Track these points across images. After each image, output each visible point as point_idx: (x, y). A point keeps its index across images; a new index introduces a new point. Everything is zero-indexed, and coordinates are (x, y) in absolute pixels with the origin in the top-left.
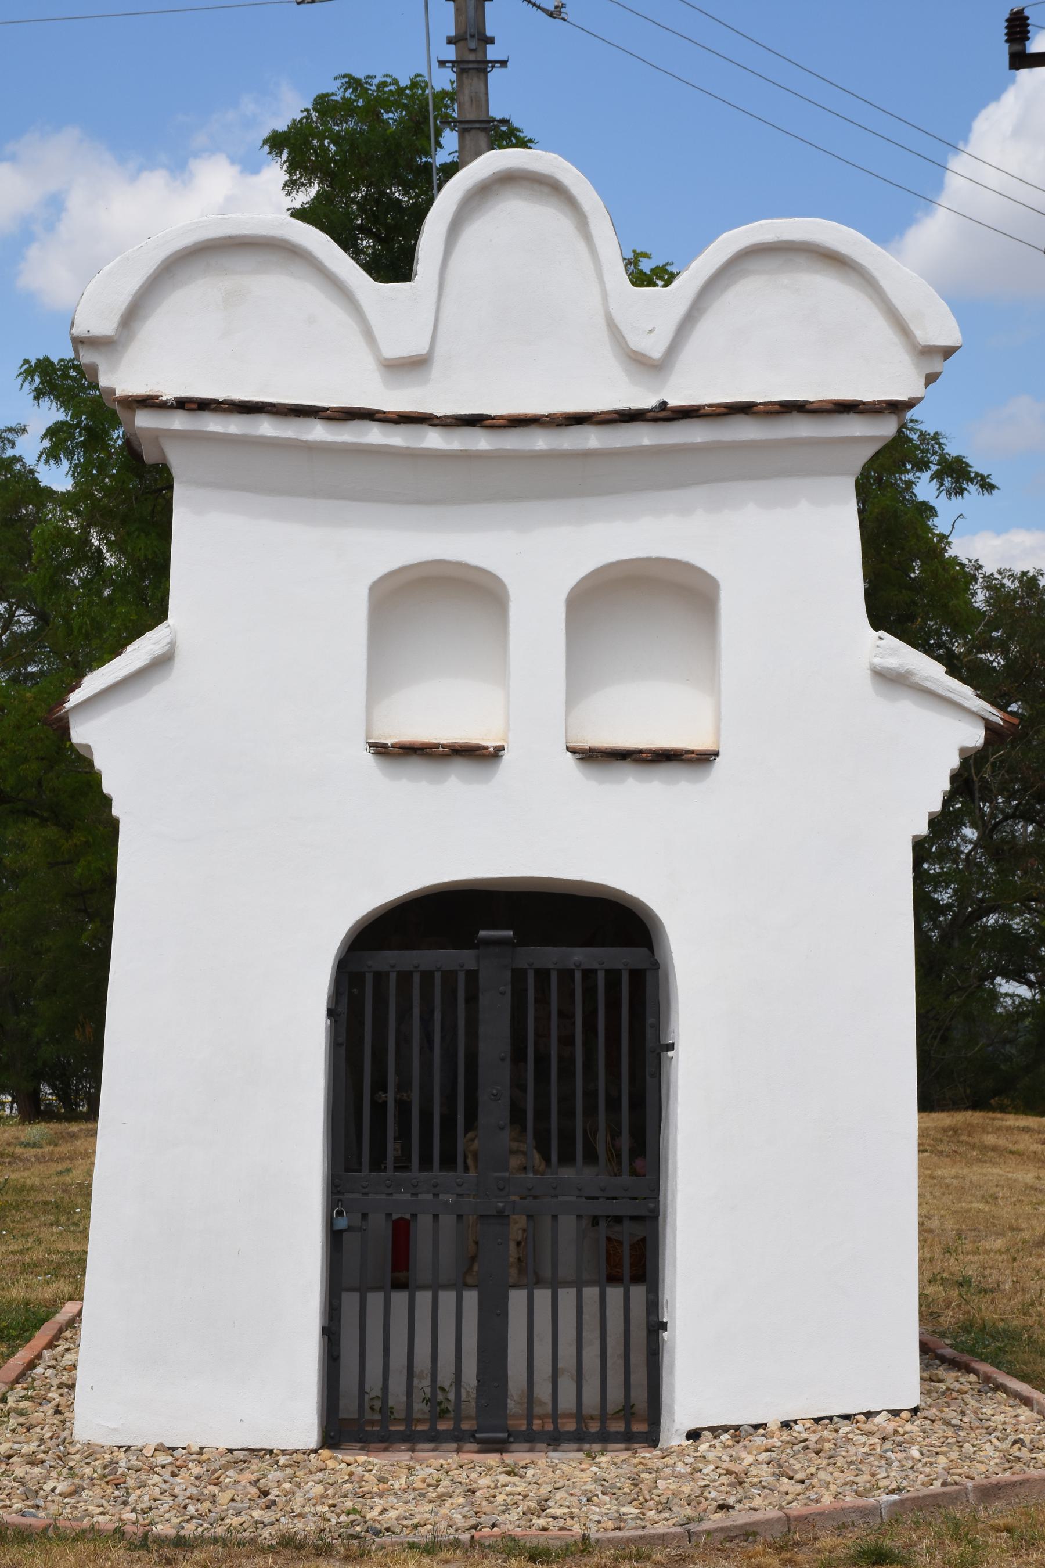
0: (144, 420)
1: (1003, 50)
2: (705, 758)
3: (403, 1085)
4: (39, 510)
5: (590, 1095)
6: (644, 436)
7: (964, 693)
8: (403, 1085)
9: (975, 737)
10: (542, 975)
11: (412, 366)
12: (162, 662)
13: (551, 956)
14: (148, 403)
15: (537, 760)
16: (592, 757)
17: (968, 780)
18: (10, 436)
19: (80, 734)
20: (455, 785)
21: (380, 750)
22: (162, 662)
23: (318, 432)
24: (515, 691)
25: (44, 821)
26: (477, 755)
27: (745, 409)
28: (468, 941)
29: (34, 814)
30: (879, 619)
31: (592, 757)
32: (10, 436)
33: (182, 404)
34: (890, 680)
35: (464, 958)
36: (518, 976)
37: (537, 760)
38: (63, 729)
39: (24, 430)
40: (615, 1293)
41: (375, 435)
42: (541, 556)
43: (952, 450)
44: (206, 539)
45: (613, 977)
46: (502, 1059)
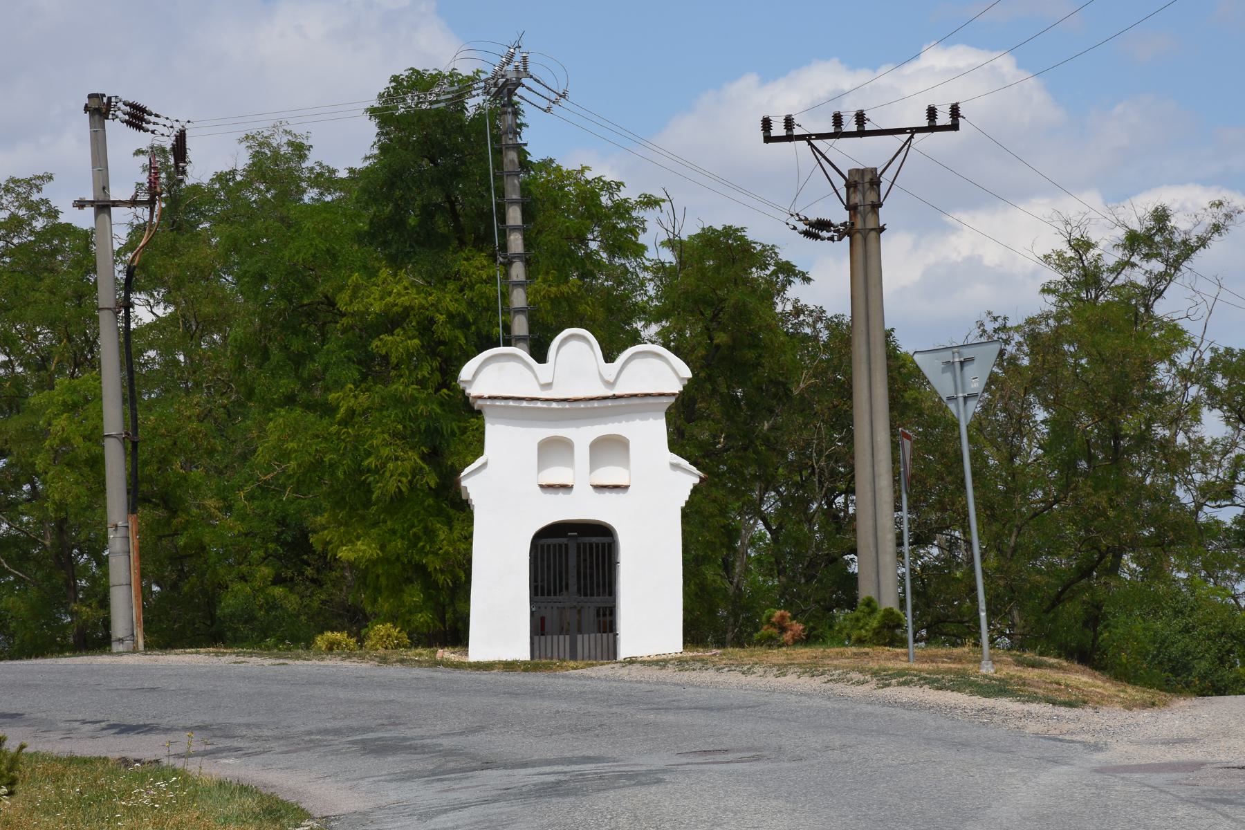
0: (480, 402)
1: (760, 134)
2: (626, 487)
3: (543, 580)
4: (61, 243)
5: (592, 584)
6: (609, 403)
7: (693, 469)
8: (543, 580)
9: (697, 481)
10: (585, 544)
11: (548, 386)
12: (484, 465)
13: (587, 540)
14: (481, 398)
15: (583, 489)
16: (598, 487)
17: (695, 490)
18: (38, 182)
19: (463, 484)
20: (561, 496)
21: (542, 486)
22: (484, 465)
23: (525, 404)
24: (577, 471)
25: (156, 506)
26: (566, 488)
27: (636, 395)
28: (566, 536)
29: (150, 502)
30: (672, 450)
31: (598, 487)
32: (38, 182)
33: (490, 398)
34: (675, 466)
35: (563, 541)
36: (578, 545)
37: (583, 489)
38: (458, 483)
39: (50, 178)
40: (605, 635)
41: (539, 404)
42: (583, 436)
43: (784, 256)
44: (496, 434)
45: (603, 545)
46: (575, 566)
